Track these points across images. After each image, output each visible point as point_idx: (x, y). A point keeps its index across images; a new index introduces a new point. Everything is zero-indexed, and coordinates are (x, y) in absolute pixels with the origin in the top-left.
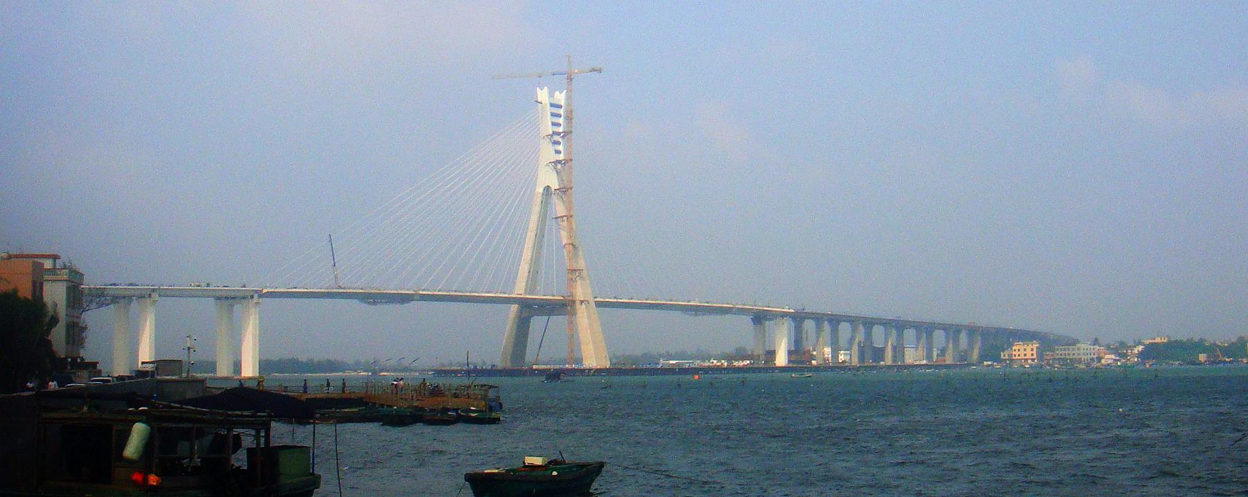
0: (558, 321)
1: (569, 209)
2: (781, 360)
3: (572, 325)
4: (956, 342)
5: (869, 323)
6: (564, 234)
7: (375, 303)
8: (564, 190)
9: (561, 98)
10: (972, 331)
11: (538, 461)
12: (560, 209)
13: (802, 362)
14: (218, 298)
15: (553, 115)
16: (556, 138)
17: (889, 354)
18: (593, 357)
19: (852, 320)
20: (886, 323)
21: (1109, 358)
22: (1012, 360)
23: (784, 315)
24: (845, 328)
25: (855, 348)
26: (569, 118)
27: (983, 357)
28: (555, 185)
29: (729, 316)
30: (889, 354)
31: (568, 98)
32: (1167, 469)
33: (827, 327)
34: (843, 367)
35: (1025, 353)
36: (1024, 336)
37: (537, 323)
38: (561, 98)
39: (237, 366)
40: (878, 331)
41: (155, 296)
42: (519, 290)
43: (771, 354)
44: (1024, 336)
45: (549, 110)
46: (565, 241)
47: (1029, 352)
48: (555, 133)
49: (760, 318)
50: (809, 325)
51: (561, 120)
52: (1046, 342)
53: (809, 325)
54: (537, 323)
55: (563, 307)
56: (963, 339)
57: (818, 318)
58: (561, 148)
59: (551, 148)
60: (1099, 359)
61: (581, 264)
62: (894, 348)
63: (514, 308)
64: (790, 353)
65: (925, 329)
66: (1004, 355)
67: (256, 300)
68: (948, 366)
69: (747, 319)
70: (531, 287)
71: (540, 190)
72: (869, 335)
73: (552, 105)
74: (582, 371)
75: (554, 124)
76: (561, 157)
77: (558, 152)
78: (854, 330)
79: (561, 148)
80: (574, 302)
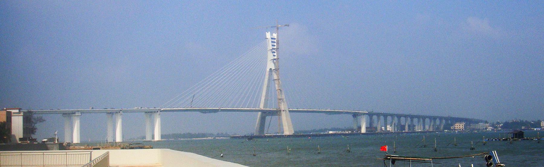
0: (275, 118)
1: (278, 77)
2: (363, 130)
3: (280, 119)
4: (435, 122)
5: (399, 116)
6: (276, 86)
7: (205, 113)
8: (276, 70)
9: (275, 35)
10: (441, 118)
11: (45, 140)
12: (275, 77)
13: (372, 131)
14: (146, 112)
15: (272, 42)
16: (273, 51)
17: (407, 127)
18: (288, 130)
19: (392, 115)
20: (406, 116)
21: (490, 129)
22: (455, 130)
23: (364, 114)
24: (389, 118)
25: (393, 125)
26: (278, 43)
27: (445, 128)
28: (273, 68)
29: (340, 115)
30: (407, 127)
31: (278, 36)
32: (131, 146)
33: (382, 118)
34: (388, 133)
35: (459, 126)
36: (460, 120)
37: (268, 118)
38: (275, 35)
39: (153, 137)
40: (403, 119)
41: (121, 112)
42: (262, 107)
43: (360, 128)
44: (460, 120)
45: (270, 40)
46: (277, 89)
47: (461, 126)
48: (273, 49)
49: (355, 115)
50: (375, 117)
51: (275, 44)
52: (468, 121)
53: (375, 117)
54: (268, 118)
55: (277, 113)
56: (438, 122)
57: (378, 115)
58: (275, 54)
59: (272, 54)
60: (486, 128)
61: (283, 96)
62: (409, 126)
63: (260, 113)
64: (367, 128)
65: (422, 118)
66: (452, 128)
67: (159, 113)
68: (430, 132)
69: (351, 116)
70: (265, 105)
71: (268, 70)
72: (399, 121)
73: (272, 38)
74: (283, 136)
75: (273, 45)
76: (276, 57)
77: (275, 56)
78: (393, 119)
79: (275, 54)
80: (280, 111)
